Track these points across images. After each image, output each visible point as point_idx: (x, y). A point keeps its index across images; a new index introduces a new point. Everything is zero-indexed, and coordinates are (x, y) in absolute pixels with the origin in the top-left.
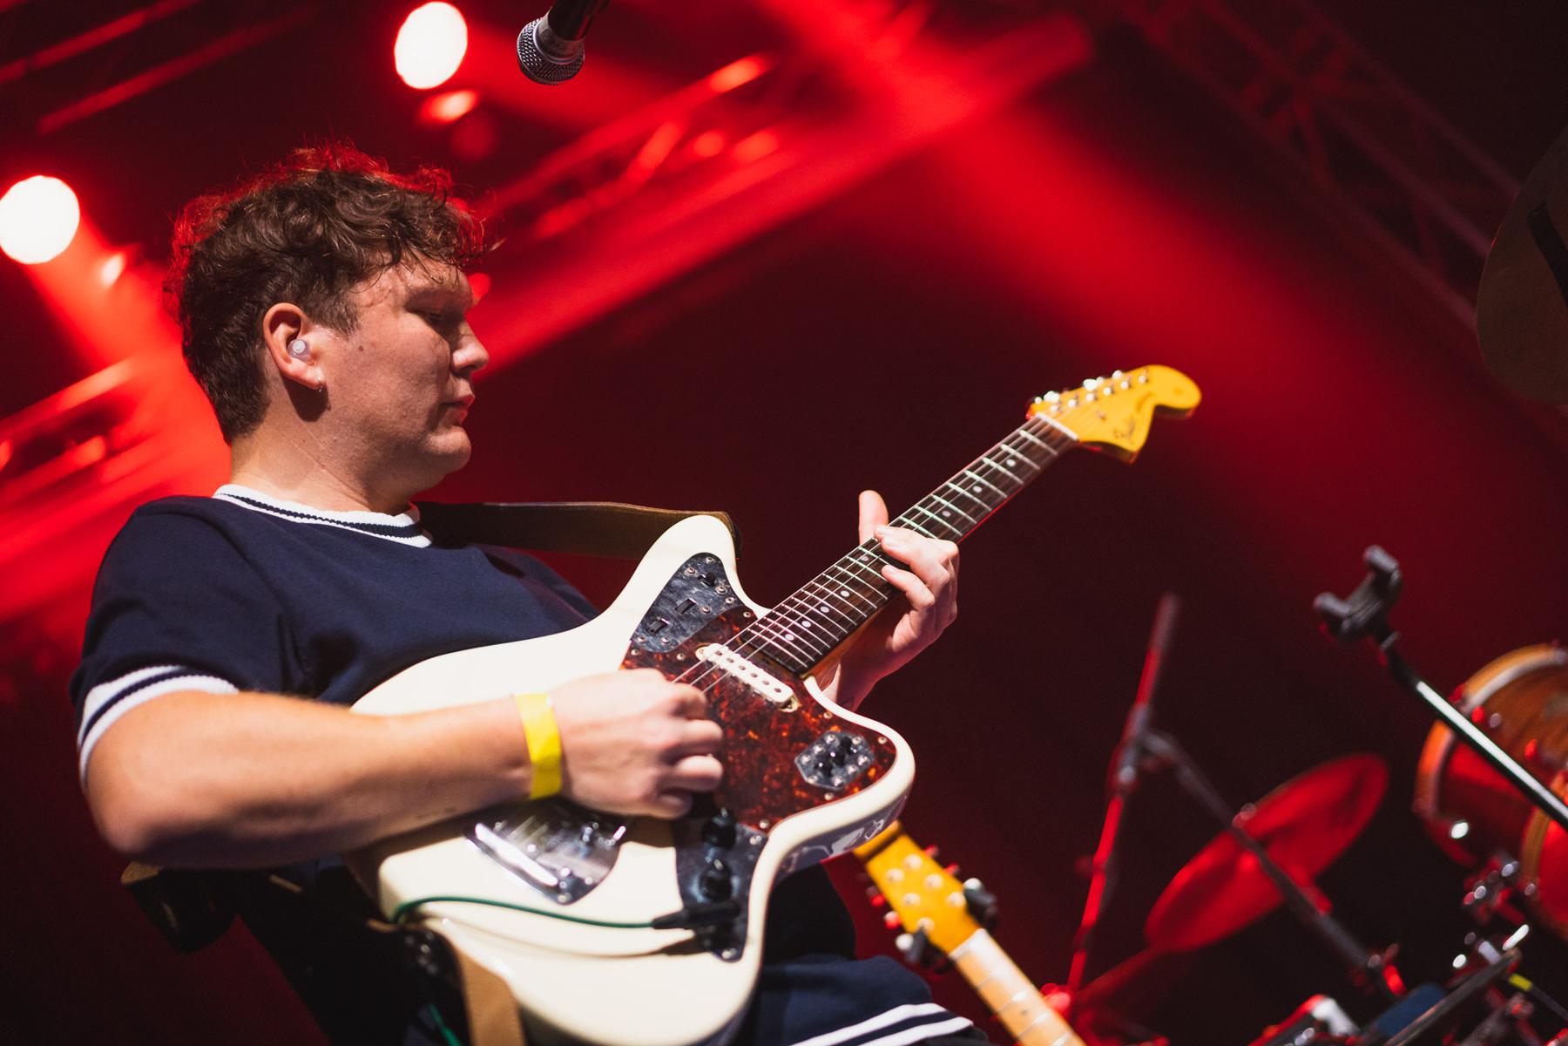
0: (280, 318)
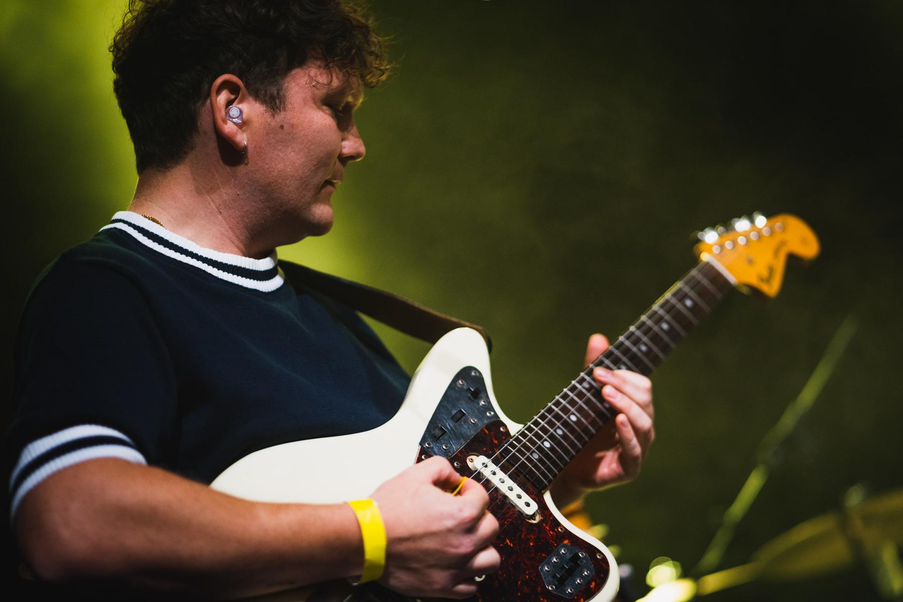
0: (226, 85)
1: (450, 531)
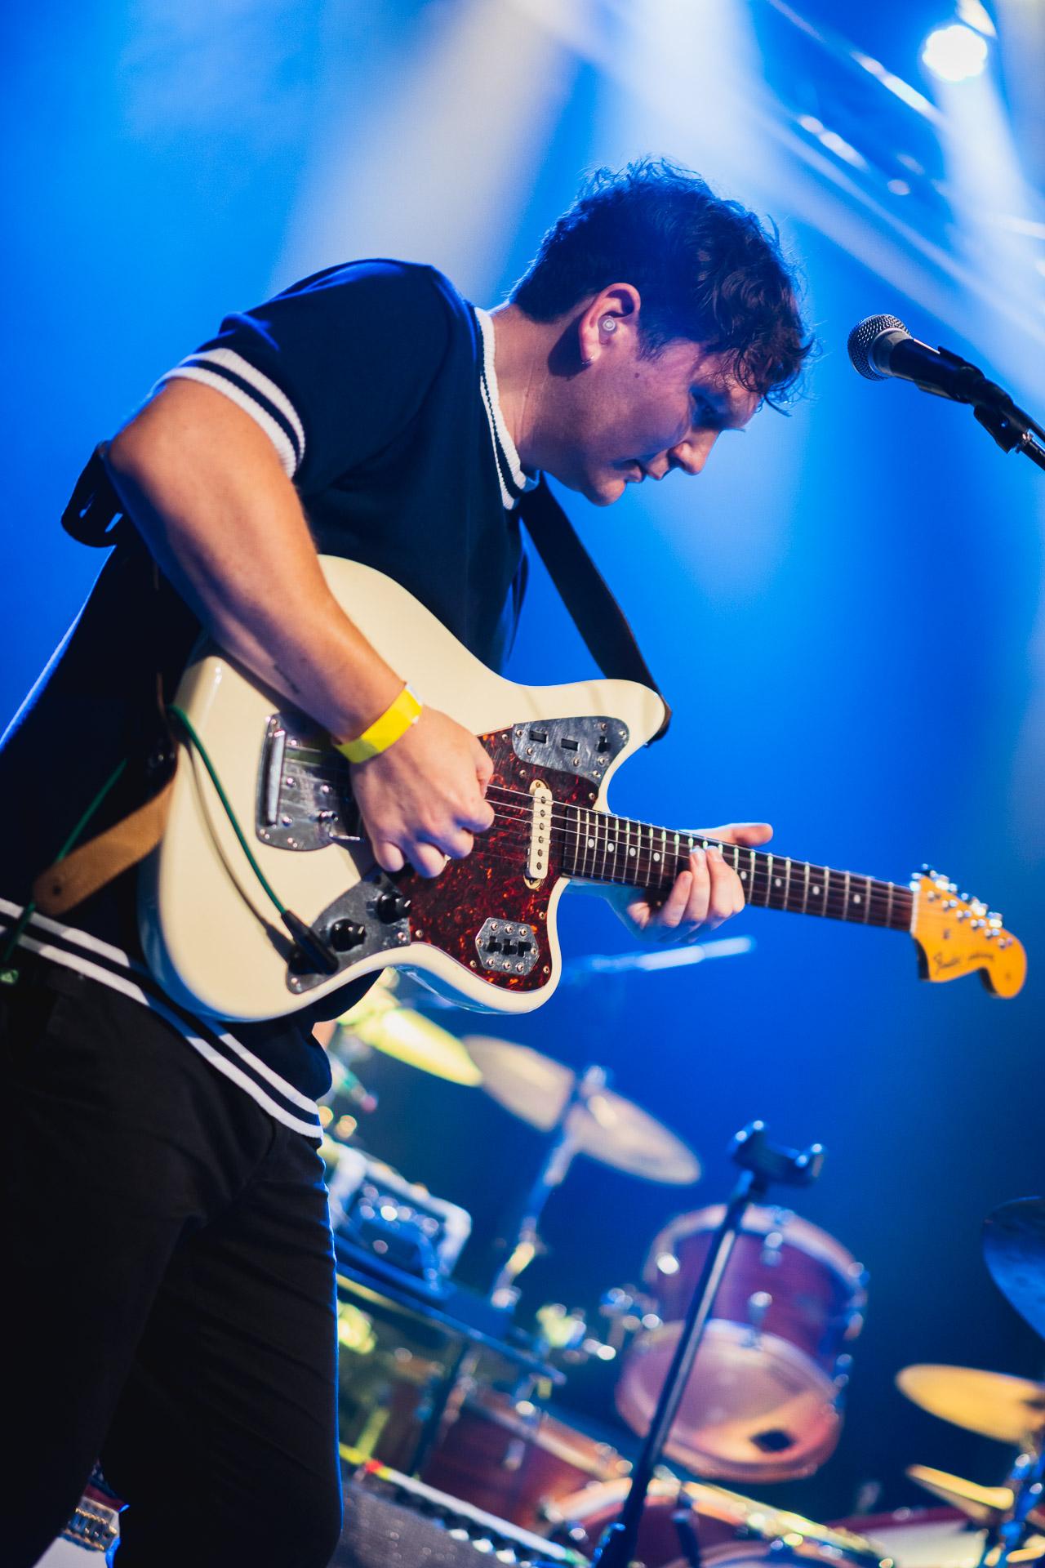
1: (446, 802)
